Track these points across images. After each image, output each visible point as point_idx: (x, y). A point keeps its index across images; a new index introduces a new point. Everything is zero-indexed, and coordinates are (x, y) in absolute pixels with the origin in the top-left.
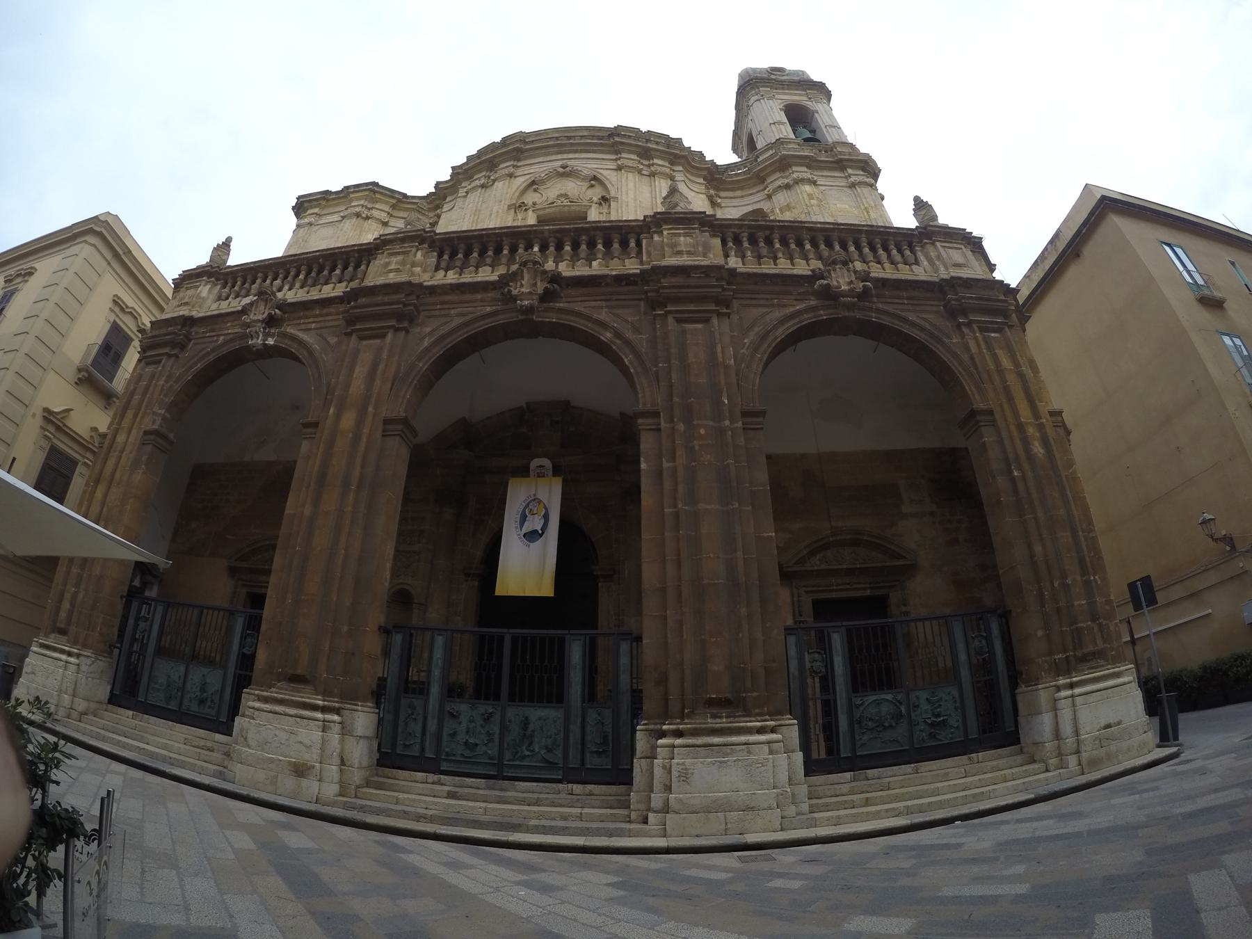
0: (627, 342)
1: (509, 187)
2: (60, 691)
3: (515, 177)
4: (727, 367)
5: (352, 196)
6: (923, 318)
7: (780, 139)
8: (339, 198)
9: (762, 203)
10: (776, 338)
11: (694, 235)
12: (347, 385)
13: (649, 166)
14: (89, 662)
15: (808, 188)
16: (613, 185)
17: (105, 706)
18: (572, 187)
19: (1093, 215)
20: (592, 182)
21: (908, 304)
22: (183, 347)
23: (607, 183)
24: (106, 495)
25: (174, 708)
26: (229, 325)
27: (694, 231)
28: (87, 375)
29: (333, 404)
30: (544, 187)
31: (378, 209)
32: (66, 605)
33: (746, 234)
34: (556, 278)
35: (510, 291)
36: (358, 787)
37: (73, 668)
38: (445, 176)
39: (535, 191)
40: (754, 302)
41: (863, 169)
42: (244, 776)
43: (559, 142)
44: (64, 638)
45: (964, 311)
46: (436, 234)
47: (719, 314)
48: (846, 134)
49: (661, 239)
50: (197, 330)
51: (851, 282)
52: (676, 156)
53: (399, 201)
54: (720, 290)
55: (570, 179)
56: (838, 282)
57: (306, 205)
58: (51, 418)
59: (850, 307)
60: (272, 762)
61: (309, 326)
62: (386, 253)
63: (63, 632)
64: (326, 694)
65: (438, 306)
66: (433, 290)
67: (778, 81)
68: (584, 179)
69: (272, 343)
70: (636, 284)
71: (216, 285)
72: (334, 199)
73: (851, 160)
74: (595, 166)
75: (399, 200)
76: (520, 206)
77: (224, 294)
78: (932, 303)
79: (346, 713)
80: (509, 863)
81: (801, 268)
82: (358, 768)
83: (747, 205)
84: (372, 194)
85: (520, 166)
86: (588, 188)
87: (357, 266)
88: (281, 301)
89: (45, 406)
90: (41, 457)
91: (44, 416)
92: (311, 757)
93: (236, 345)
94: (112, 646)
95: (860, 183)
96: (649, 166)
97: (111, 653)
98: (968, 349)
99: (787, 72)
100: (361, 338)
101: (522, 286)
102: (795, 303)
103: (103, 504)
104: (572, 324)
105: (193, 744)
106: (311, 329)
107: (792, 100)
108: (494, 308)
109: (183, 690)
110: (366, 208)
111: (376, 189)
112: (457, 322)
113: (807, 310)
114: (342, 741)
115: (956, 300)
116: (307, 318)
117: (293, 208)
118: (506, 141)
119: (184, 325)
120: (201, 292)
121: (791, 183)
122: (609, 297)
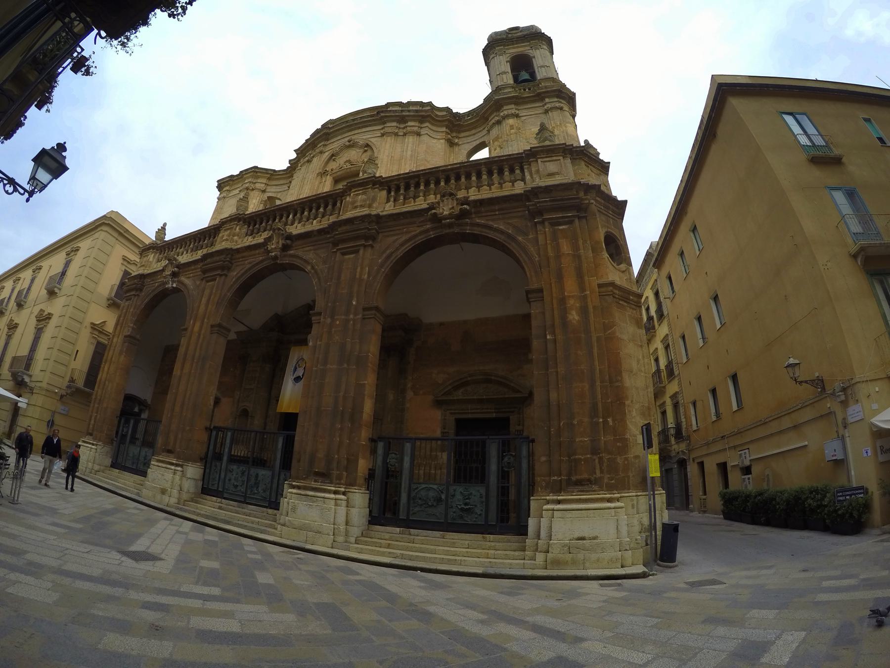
1: (319, 160)
2: (88, 461)
3: (324, 153)
5: (245, 176)
7: (498, 86)
9: (485, 137)
10: (397, 256)
14: (100, 447)
15: (511, 121)
16: (377, 149)
17: (108, 469)
18: (354, 155)
19: (717, 101)
20: (365, 148)
21: (499, 214)
22: (141, 290)
24: (109, 369)
26: (159, 277)
27: (367, 190)
28: (112, 302)
30: (339, 157)
31: (259, 183)
32: (92, 422)
34: (289, 237)
36: (185, 501)
37: (94, 451)
38: (294, 156)
39: (334, 160)
40: (392, 233)
41: (558, 97)
42: (147, 495)
43: (348, 124)
44: (91, 437)
45: (540, 213)
46: (246, 215)
50: (147, 280)
51: (453, 208)
52: (423, 117)
53: (272, 175)
55: (354, 149)
58: (95, 327)
59: (450, 226)
60: (155, 488)
63: (91, 435)
64: (178, 458)
65: (241, 260)
67: (508, 40)
68: (361, 147)
69: (175, 286)
70: (328, 233)
71: (157, 253)
72: (236, 179)
73: (548, 92)
74: (368, 136)
75: (271, 174)
76: (324, 173)
77: (160, 258)
78: (519, 209)
79: (184, 467)
82: (186, 492)
83: (476, 140)
84: (255, 174)
85: (328, 144)
89: (91, 322)
90: (92, 348)
91: (91, 327)
92: (167, 486)
93: (161, 288)
94: (112, 440)
95: (552, 109)
97: (112, 443)
99: (521, 29)
103: (108, 373)
105: (137, 482)
107: (518, 52)
109: (138, 459)
110: (252, 183)
111: (257, 170)
112: (248, 266)
114: (181, 479)
115: (533, 205)
116: (189, 271)
117: (217, 187)
118: (313, 136)
119: (141, 278)
120: (150, 258)
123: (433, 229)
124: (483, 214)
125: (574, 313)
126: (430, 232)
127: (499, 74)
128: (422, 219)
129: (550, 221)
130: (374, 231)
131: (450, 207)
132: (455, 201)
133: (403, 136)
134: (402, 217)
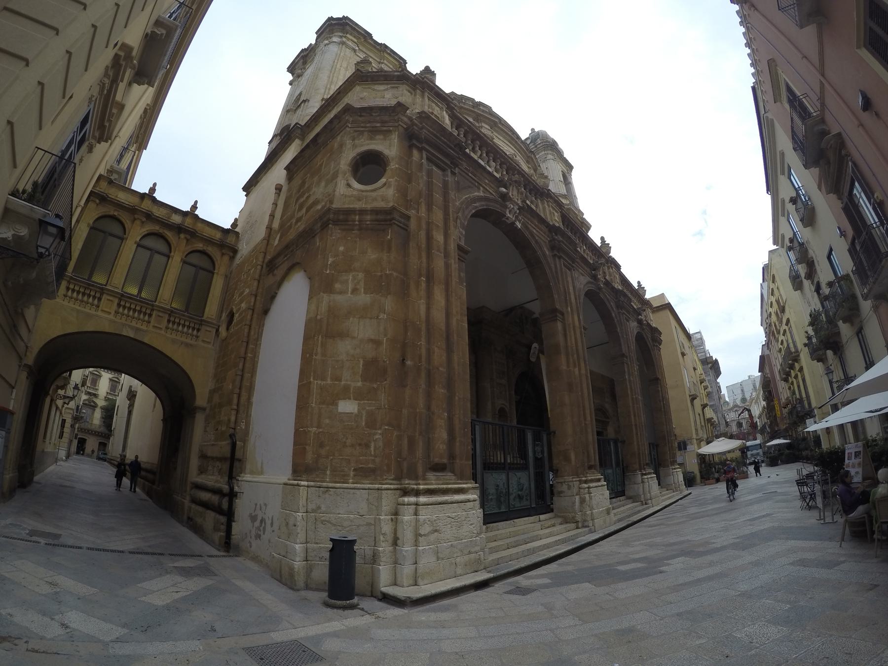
8: (375, 47)
25: (505, 510)
48: (582, 208)
57: (348, 28)
72: (370, 44)
80: (559, 581)
96: (379, 63)
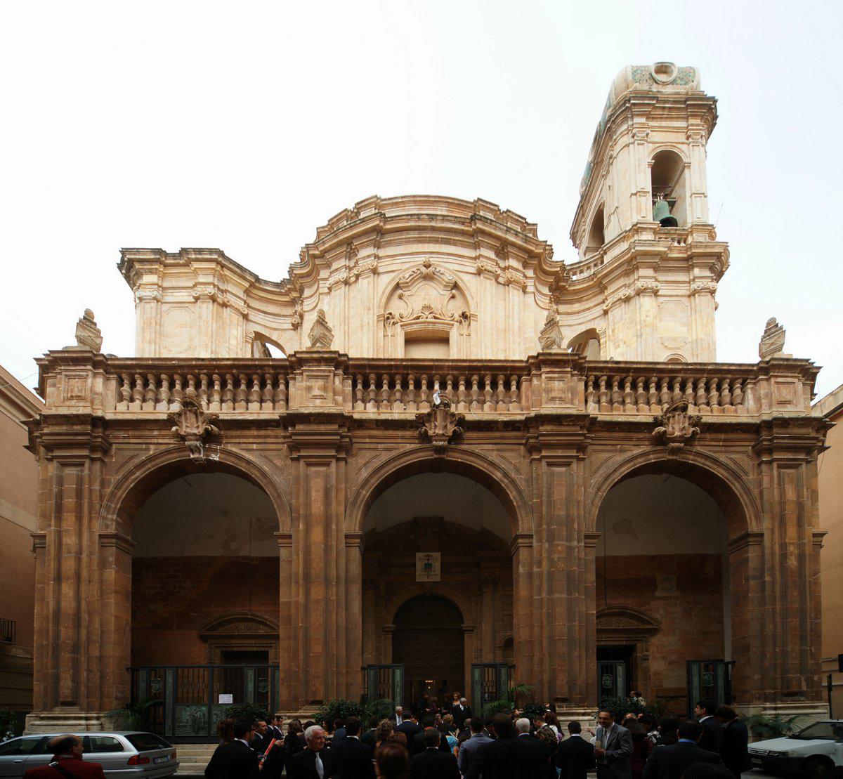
0: (512, 481)
4: (578, 502)
6: (731, 459)
9: (597, 321)
11: (566, 380)
12: (308, 505)
13: (504, 269)
23: (467, 293)
27: (565, 375)
29: (301, 521)
33: (605, 378)
34: (461, 422)
35: (426, 432)
45: (770, 451)
47: (578, 459)
49: (539, 383)
51: (683, 429)
54: (583, 438)
55: (433, 285)
56: (673, 428)
61: (251, 446)
62: (305, 374)
66: (362, 424)
81: (645, 414)
84: (219, 268)
86: (449, 299)
87: (275, 385)
88: (214, 417)
98: (760, 484)
100: (309, 465)
101: (436, 426)
102: (633, 448)
104: (472, 464)
106: (253, 450)
108: (412, 445)
113: (641, 455)
121: (633, 293)
122: (499, 441)
123: (654, 452)
124: (707, 443)
125: (793, 558)
126: (650, 455)
127: (636, 194)
128: (641, 436)
129: (779, 463)
130: (100, 440)
131: (681, 426)
132: (687, 421)
133: (504, 285)
134: (617, 429)
